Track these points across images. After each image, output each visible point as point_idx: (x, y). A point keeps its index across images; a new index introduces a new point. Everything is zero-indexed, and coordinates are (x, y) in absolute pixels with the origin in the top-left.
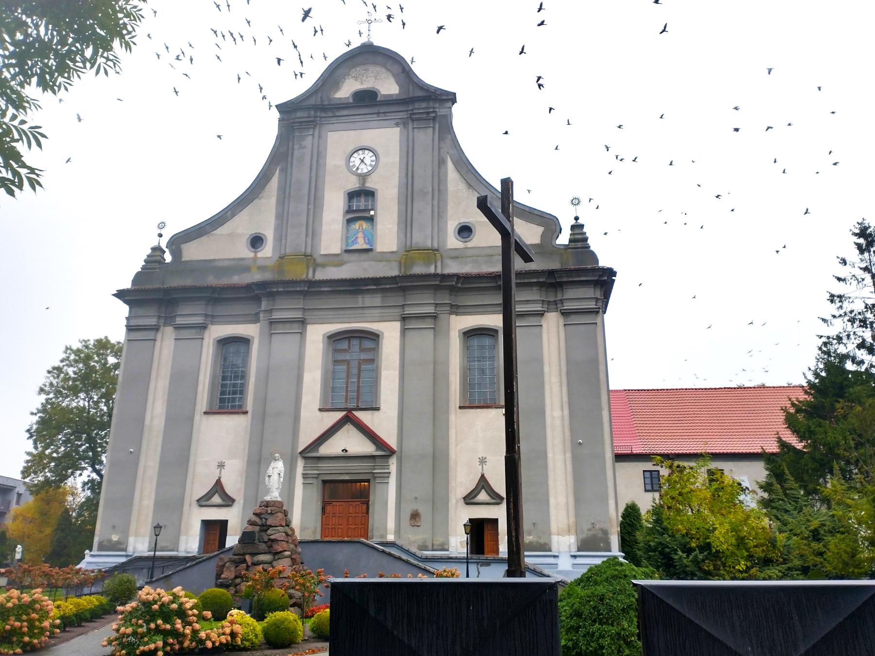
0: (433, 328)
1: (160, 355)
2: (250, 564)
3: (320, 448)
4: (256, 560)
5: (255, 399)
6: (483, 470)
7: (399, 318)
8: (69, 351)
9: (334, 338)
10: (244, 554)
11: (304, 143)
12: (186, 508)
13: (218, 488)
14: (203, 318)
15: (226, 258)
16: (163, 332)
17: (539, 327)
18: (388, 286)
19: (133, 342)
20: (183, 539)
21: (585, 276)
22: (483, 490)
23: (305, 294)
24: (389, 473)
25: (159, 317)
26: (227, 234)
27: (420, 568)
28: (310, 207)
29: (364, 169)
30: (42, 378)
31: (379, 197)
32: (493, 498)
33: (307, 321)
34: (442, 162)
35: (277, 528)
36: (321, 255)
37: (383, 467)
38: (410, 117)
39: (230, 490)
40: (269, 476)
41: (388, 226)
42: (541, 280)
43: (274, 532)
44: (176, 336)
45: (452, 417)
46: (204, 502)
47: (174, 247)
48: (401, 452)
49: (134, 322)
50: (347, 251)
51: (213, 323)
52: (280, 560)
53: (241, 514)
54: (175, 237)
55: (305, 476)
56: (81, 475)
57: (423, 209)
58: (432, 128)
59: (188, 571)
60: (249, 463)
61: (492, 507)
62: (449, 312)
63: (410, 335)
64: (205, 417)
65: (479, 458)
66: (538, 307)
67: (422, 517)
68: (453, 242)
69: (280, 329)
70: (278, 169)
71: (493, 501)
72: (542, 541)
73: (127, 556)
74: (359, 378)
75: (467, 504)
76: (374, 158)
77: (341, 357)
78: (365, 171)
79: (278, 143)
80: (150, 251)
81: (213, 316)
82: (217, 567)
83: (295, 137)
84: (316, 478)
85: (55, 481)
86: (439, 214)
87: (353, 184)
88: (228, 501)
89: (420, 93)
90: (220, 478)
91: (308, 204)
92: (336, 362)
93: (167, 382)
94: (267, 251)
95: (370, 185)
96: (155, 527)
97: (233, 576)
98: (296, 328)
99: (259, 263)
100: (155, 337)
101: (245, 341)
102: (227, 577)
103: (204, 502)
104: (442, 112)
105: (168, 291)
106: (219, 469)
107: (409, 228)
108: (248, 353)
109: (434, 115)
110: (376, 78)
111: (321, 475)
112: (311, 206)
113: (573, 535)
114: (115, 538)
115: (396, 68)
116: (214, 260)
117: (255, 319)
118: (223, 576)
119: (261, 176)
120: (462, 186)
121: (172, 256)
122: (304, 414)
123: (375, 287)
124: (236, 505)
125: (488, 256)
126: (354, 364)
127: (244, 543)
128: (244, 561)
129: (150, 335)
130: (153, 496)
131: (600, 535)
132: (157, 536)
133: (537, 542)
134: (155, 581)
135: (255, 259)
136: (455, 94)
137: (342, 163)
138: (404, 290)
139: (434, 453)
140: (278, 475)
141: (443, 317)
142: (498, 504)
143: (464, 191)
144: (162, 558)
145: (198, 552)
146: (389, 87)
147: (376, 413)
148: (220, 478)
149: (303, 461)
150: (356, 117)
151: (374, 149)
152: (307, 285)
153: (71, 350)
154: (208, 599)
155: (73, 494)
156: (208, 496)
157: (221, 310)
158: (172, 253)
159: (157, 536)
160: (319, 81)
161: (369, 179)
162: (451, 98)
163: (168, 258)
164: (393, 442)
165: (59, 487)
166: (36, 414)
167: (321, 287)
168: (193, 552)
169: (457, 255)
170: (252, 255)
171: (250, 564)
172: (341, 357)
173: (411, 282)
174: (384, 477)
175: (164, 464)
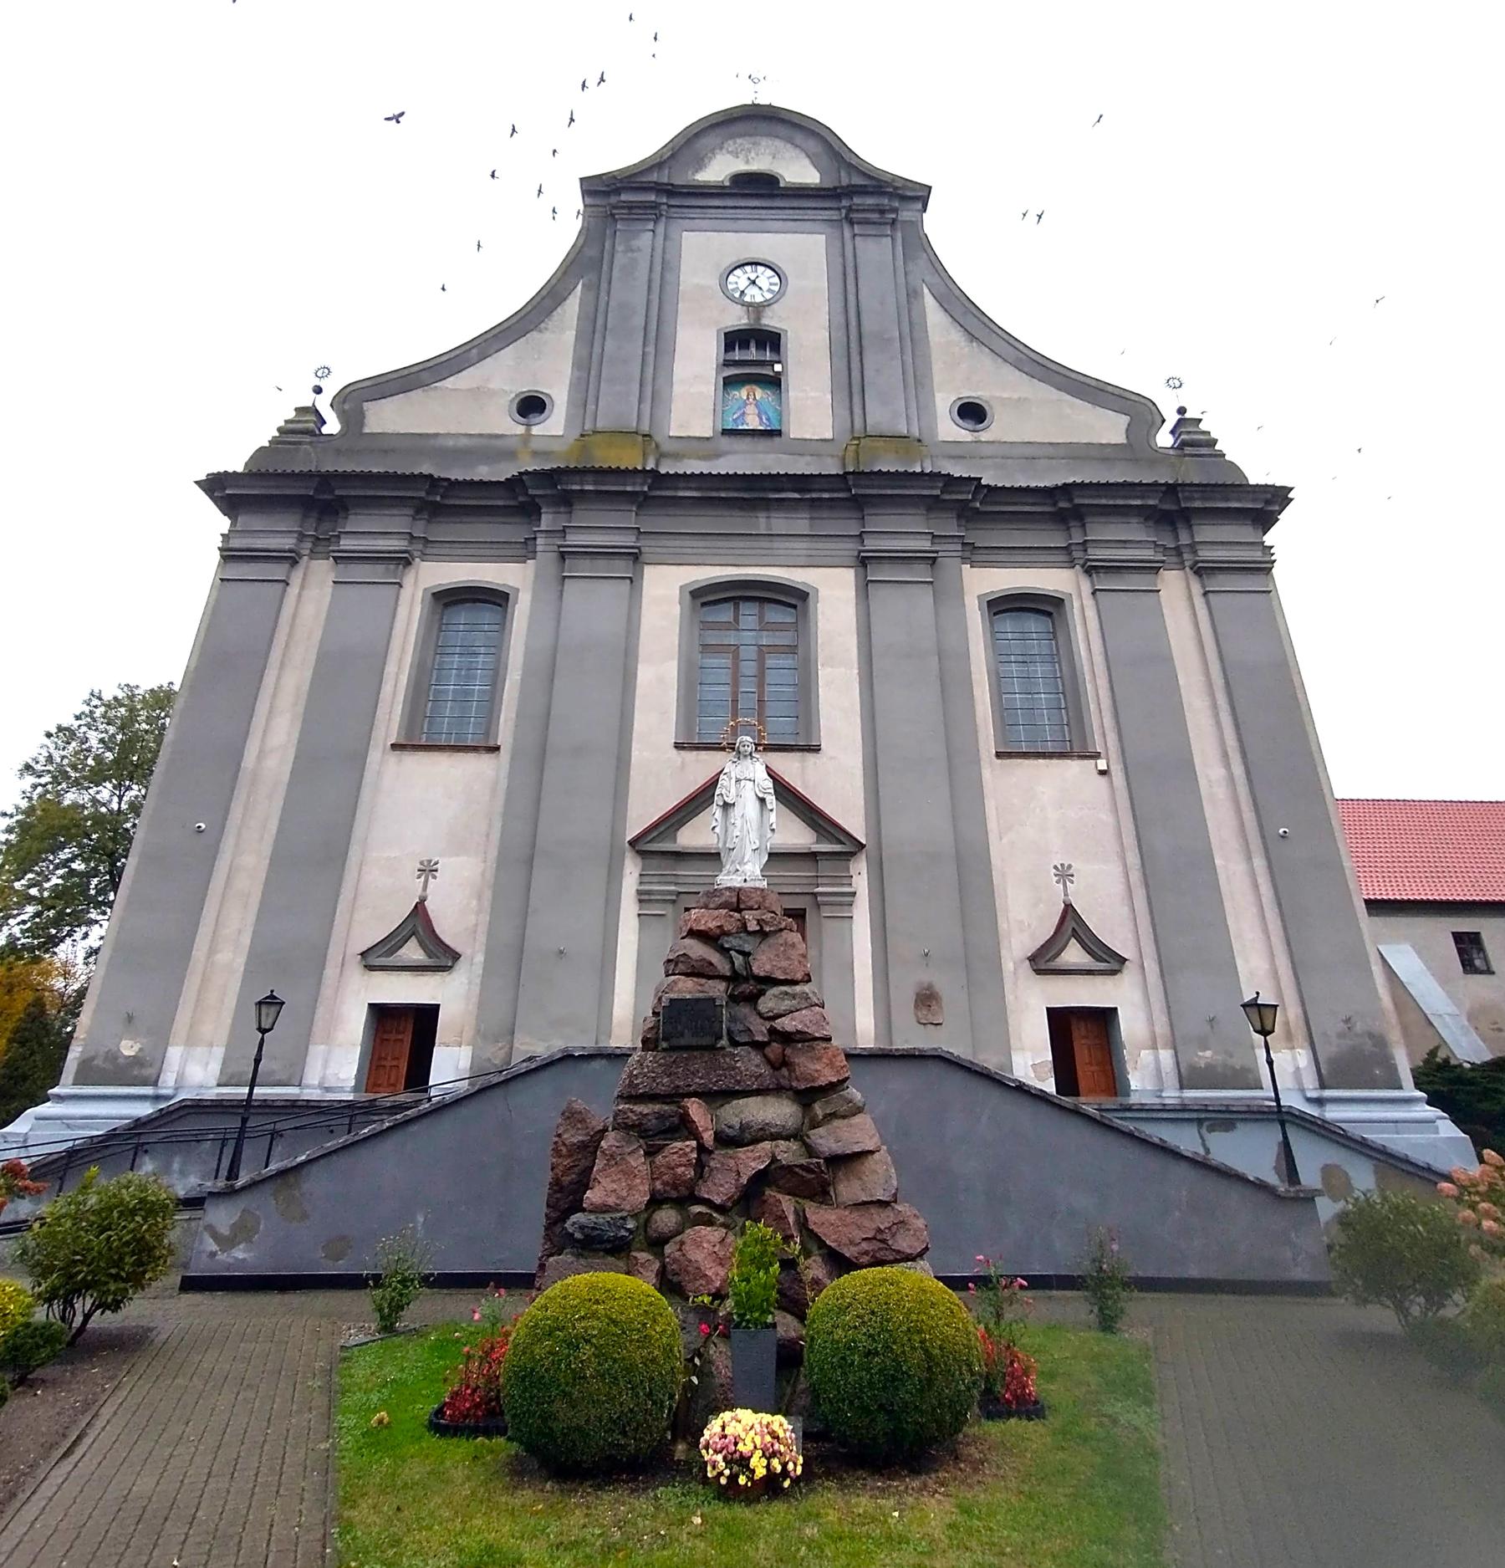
0: (931, 582)
1: (294, 616)
2: (708, 1137)
3: (679, 833)
4: (735, 1122)
5: (520, 715)
6: (1066, 895)
7: (852, 561)
8: (95, 702)
9: (704, 597)
10: (675, 1096)
11: (635, 243)
12: (330, 972)
13: (418, 922)
14: (406, 543)
15: (463, 432)
16: (307, 568)
17: (1156, 594)
18: (826, 495)
19: (256, 583)
20: (316, 1051)
21: (1239, 500)
22: (1073, 940)
23: (642, 502)
24: (854, 894)
25: (302, 537)
26: (469, 390)
27: (1144, 1140)
28: (647, 350)
29: (755, 295)
30: (33, 746)
31: (790, 345)
32: (1099, 959)
33: (643, 558)
34: (913, 295)
35: (798, 988)
36: (670, 437)
37: (838, 881)
38: (846, 217)
39: (446, 929)
40: (726, 806)
41: (812, 394)
42: (1151, 502)
43: (787, 1004)
44: (336, 577)
45: (986, 774)
46: (377, 958)
47: (346, 407)
48: (880, 848)
49: (236, 543)
50: (726, 432)
51: (424, 557)
52: (837, 1123)
53: (476, 989)
54: (351, 388)
55: (643, 897)
56: (86, 936)
57: (883, 371)
58: (889, 238)
59: (363, 1152)
60: (502, 862)
61: (1099, 979)
62: (959, 554)
63: (878, 594)
64: (393, 758)
65: (1056, 867)
66: (1147, 554)
67: (945, 1001)
68: (949, 429)
69: (584, 567)
70: (580, 287)
71: (1102, 966)
72: (1237, 1062)
73: (157, 1098)
74: (761, 685)
75: (1039, 972)
76: (776, 280)
77: (713, 638)
78: (759, 299)
79: (581, 241)
80: (294, 414)
81: (426, 541)
82: (557, 1152)
83: (618, 233)
84: (674, 902)
85: (31, 949)
86: (917, 381)
87: (737, 319)
88: (442, 958)
89: (858, 180)
90: (422, 900)
91: (644, 345)
92: (706, 648)
93: (308, 674)
94: (554, 425)
95: (770, 321)
96: (260, 1003)
97: (641, 1198)
98: (621, 568)
99: (535, 445)
100: (288, 577)
101: (496, 599)
102: (611, 1201)
103: (377, 958)
104: (905, 215)
105: (327, 480)
106: (423, 878)
107: (857, 399)
108: (503, 625)
109: (894, 216)
110: (774, 158)
111: (682, 896)
112: (651, 349)
113: (1302, 1048)
114: (128, 1048)
115: (813, 145)
116: (436, 435)
117: (525, 551)
118: (592, 1196)
119: (544, 293)
120: (956, 335)
121: (341, 423)
122: (639, 754)
123: (796, 496)
124: (462, 967)
125: (1027, 458)
126: (748, 653)
127: (672, 1049)
128: (684, 1127)
129: (277, 571)
130: (246, 940)
131: (1368, 1046)
132: (264, 1031)
133: (1225, 1066)
134: (243, 1188)
135: (527, 437)
136: (930, 188)
137: (714, 283)
138: (859, 505)
139: (957, 852)
140: (757, 804)
141: (948, 564)
142: (1114, 972)
143: (963, 344)
144: (268, 1106)
145: (355, 1089)
146: (798, 170)
147: (810, 757)
148: (422, 900)
149: (639, 860)
150: (738, 211)
151: (773, 263)
152: (649, 481)
153: (100, 699)
154: (587, 1351)
155: (66, 974)
156: (392, 942)
157: (444, 531)
158: (343, 416)
159: (264, 1031)
160: (665, 150)
161: (768, 312)
162: (919, 195)
163: (332, 426)
164: (856, 825)
165: (37, 960)
166: (11, 816)
167: (677, 489)
168: (341, 1089)
169: (956, 451)
170: (521, 430)
171: (708, 1137)
172: (713, 638)
173: (880, 487)
174: (841, 904)
175: (282, 861)
